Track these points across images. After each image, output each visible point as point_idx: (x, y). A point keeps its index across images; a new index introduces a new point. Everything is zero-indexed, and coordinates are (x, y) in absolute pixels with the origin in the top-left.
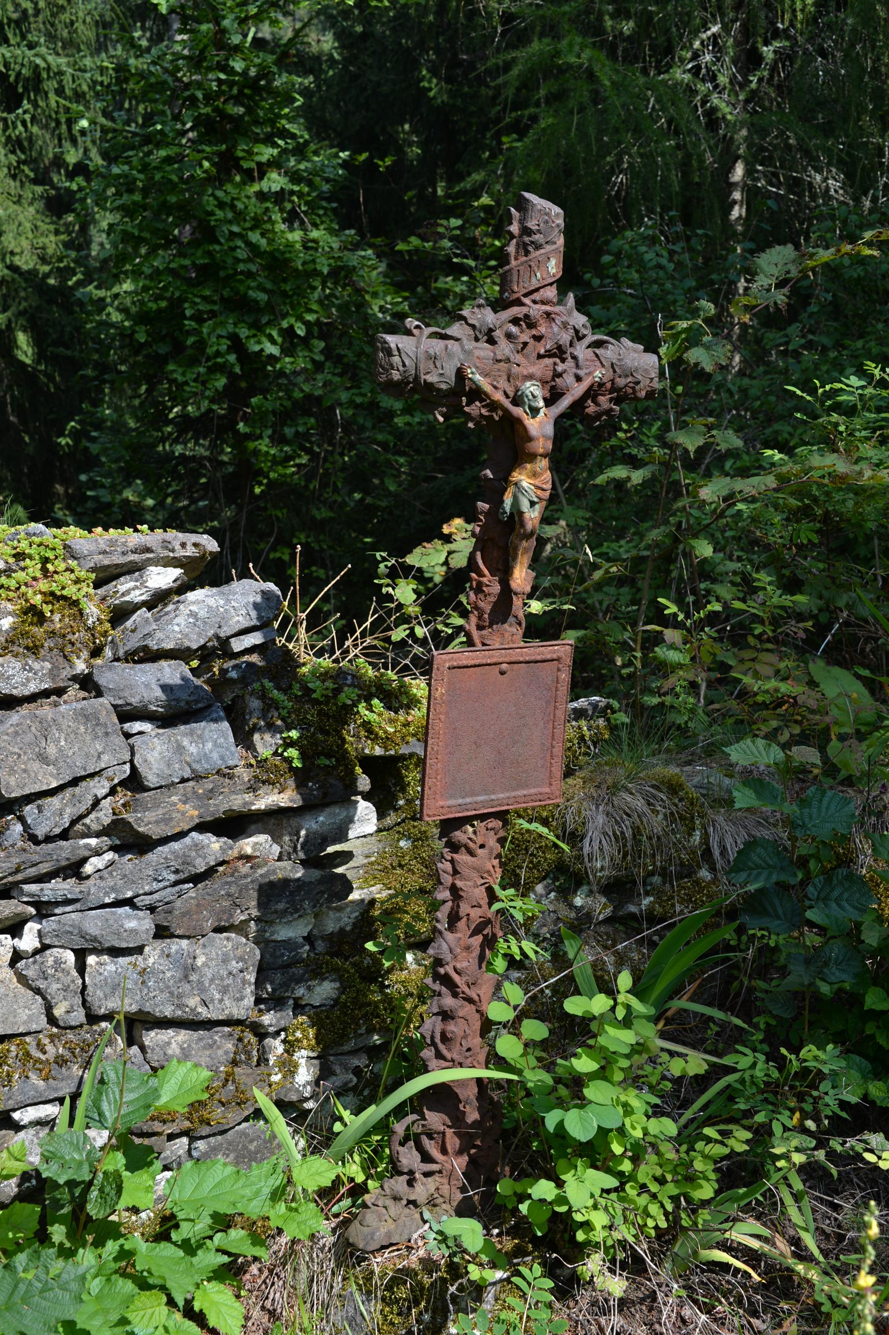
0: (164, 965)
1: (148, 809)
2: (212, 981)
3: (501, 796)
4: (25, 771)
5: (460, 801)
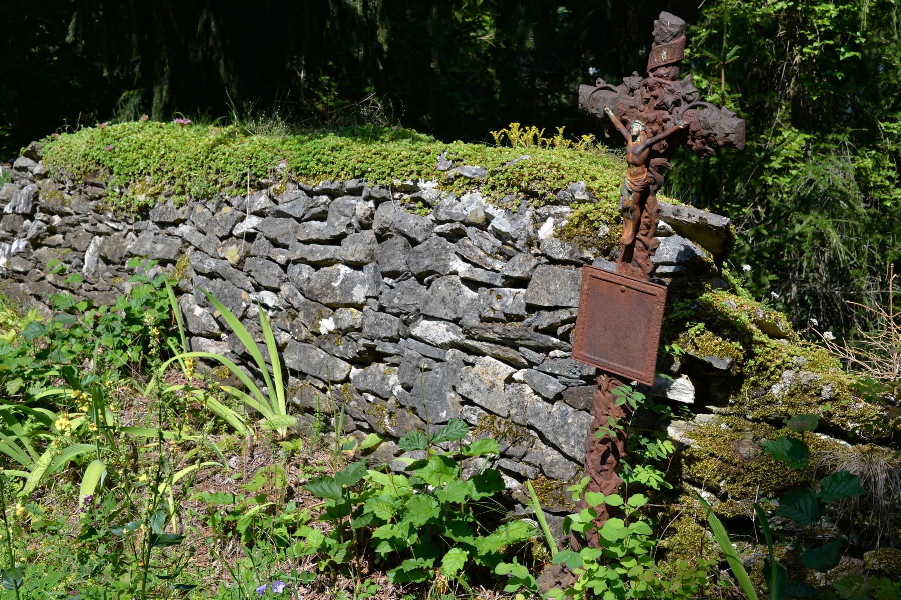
0: (557, 414)
2: (573, 434)
3: (615, 364)
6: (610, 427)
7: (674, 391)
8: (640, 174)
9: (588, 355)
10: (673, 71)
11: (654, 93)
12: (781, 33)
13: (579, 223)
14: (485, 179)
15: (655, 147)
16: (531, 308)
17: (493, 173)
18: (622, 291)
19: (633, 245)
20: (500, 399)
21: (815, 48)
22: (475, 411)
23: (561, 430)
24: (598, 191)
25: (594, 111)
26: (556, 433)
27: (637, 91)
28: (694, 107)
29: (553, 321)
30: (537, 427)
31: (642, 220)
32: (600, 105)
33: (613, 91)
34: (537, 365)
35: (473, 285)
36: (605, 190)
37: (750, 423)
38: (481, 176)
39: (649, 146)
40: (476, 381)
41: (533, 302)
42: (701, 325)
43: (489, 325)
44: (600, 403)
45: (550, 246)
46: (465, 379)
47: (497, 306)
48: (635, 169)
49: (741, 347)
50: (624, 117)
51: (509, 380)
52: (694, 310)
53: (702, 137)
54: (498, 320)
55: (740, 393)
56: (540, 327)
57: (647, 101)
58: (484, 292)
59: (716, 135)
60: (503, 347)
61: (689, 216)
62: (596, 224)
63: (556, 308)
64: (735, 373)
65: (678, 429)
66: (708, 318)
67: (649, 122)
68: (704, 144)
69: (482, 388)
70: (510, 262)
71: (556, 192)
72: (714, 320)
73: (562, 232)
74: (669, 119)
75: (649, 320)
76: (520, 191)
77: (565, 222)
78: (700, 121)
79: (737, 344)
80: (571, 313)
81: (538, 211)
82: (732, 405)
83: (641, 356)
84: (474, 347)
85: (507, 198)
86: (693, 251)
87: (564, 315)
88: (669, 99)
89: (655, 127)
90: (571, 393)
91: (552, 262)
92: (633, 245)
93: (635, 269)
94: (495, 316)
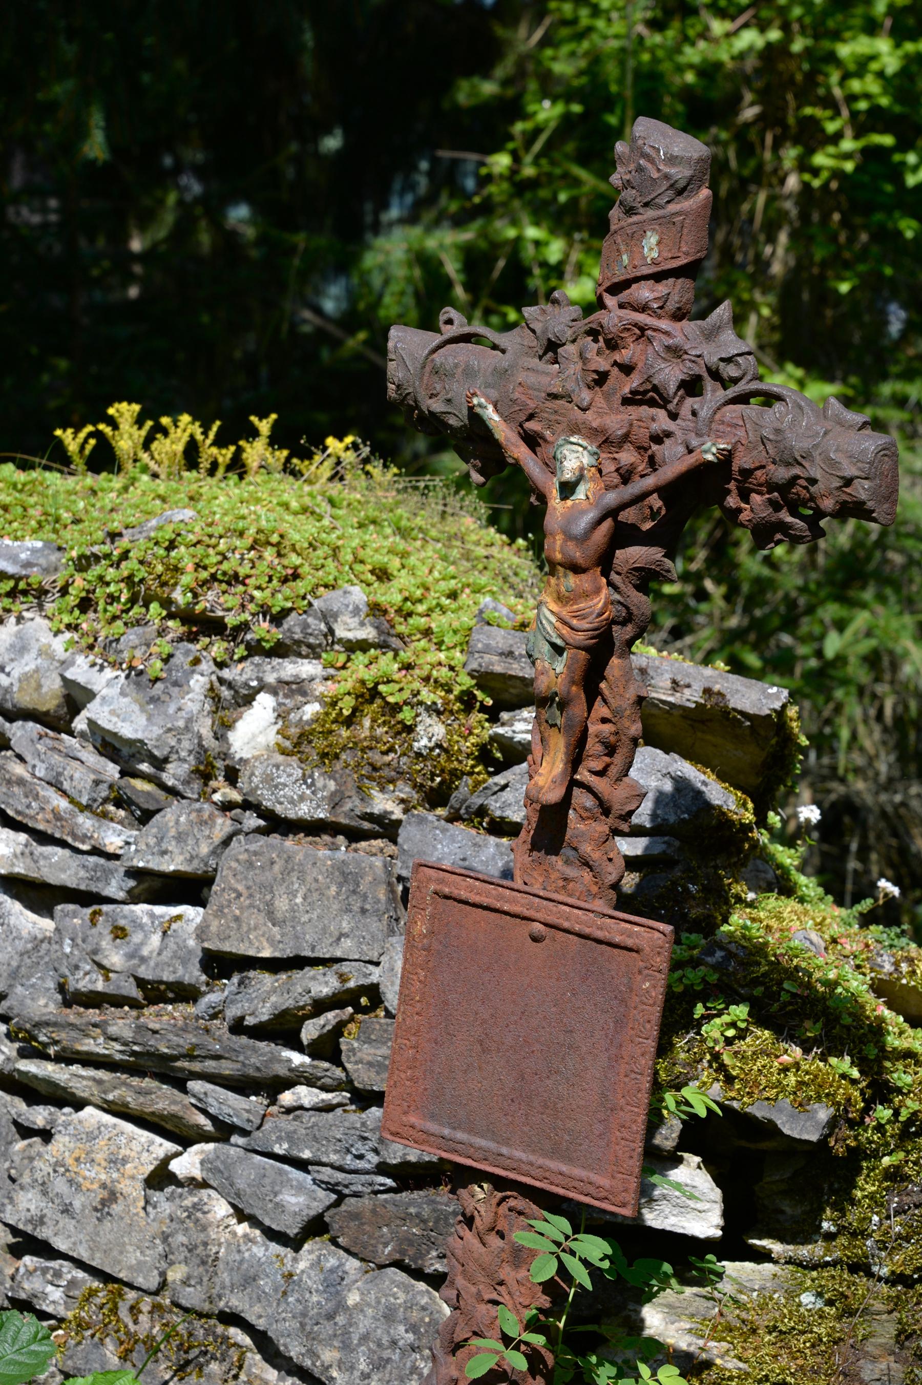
0: (313, 1281)
1: (368, 1041)
2: (365, 1338)
3: (519, 1154)
4: (237, 919)
5: (446, 1132)
6: (506, 1340)
7: (665, 1206)
8: (586, 595)
9: (432, 1127)
10: (677, 291)
11: (623, 356)
12: (749, 113)
13: (355, 710)
14: (60, 578)
15: (628, 516)
16: (220, 965)
17: (84, 563)
18: (536, 939)
19: (566, 802)
20: (136, 1237)
21: (847, 156)
22: (58, 1274)
23: (327, 1328)
24: (399, 611)
25: (437, 406)
26: (312, 1337)
27: (570, 349)
28: (743, 399)
29: (289, 1003)
30: (251, 1318)
31: (593, 729)
32: (457, 389)
33: (495, 347)
34: (245, 1133)
35: (38, 895)
36: (421, 608)
37: (884, 1288)
38: (46, 571)
39: (612, 513)
40: (60, 1185)
41: (227, 947)
42: (740, 1011)
43: (93, 1014)
44: (472, 1267)
45: (268, 779)
46: (26, 1179)
47: (115, 958)
48: (572, 581)
49: (855, 1073)
50: (532, 425)
51: (160, 1178)
52: (715, 967)
53: (772, 487)
54: (118, 1001)
55: (853, 1202)
56: (250, 1021)
57: (601, 378)
58: (75, 916)
59: (813, 481)
60: (135, 1081)
61: (676, 686)
62: (406, 715)
63: (297, 963)
64: (840, 1150)
65: (674, 1313)
66: (758, 991)
67: (607, 442)
68: (776, 507)
69: (77, 1204)
70: (152, 827)
71: (278, 619)
72: (774, 996)
73: (304, 738)
74: (668, 434)
75: (620, 1023)
76: (171, 616)
77: (311, 710)
78: (763, 440)
79: (844, 1064)
80: (343, 978)
81: (226, 674)
82: (830, 1237)
83: (598, 1128)
84: (49, 1082)
85: (132, 636)
86: (699, 793)
87: (323, 984)
88: (670, 375)
89: (627, 456)
90: (355, 1216)
91: (277, 825)
92: (566, 802)
93: (571, 872)
94: (111, 989)
